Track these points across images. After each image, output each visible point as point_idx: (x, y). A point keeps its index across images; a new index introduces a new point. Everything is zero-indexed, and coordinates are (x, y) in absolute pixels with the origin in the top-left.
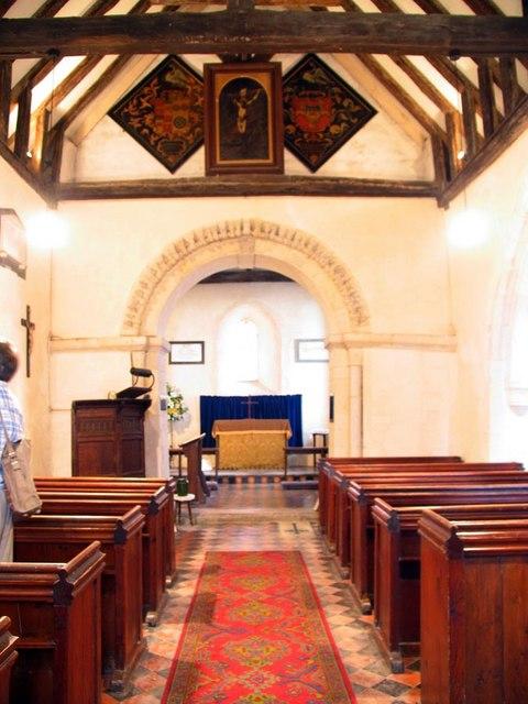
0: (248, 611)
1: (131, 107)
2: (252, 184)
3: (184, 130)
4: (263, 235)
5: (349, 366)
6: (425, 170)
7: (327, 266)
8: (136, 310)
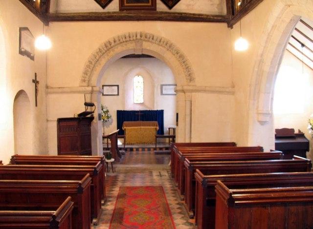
0: (138, 217)
2: (141, 15)
4: (146, 39)
5: (186, 101)
6: (222, 9)
7: (176, 54)
8: (87, 75)
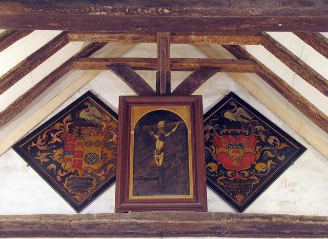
2: (170, 222)
3: (95, 167)
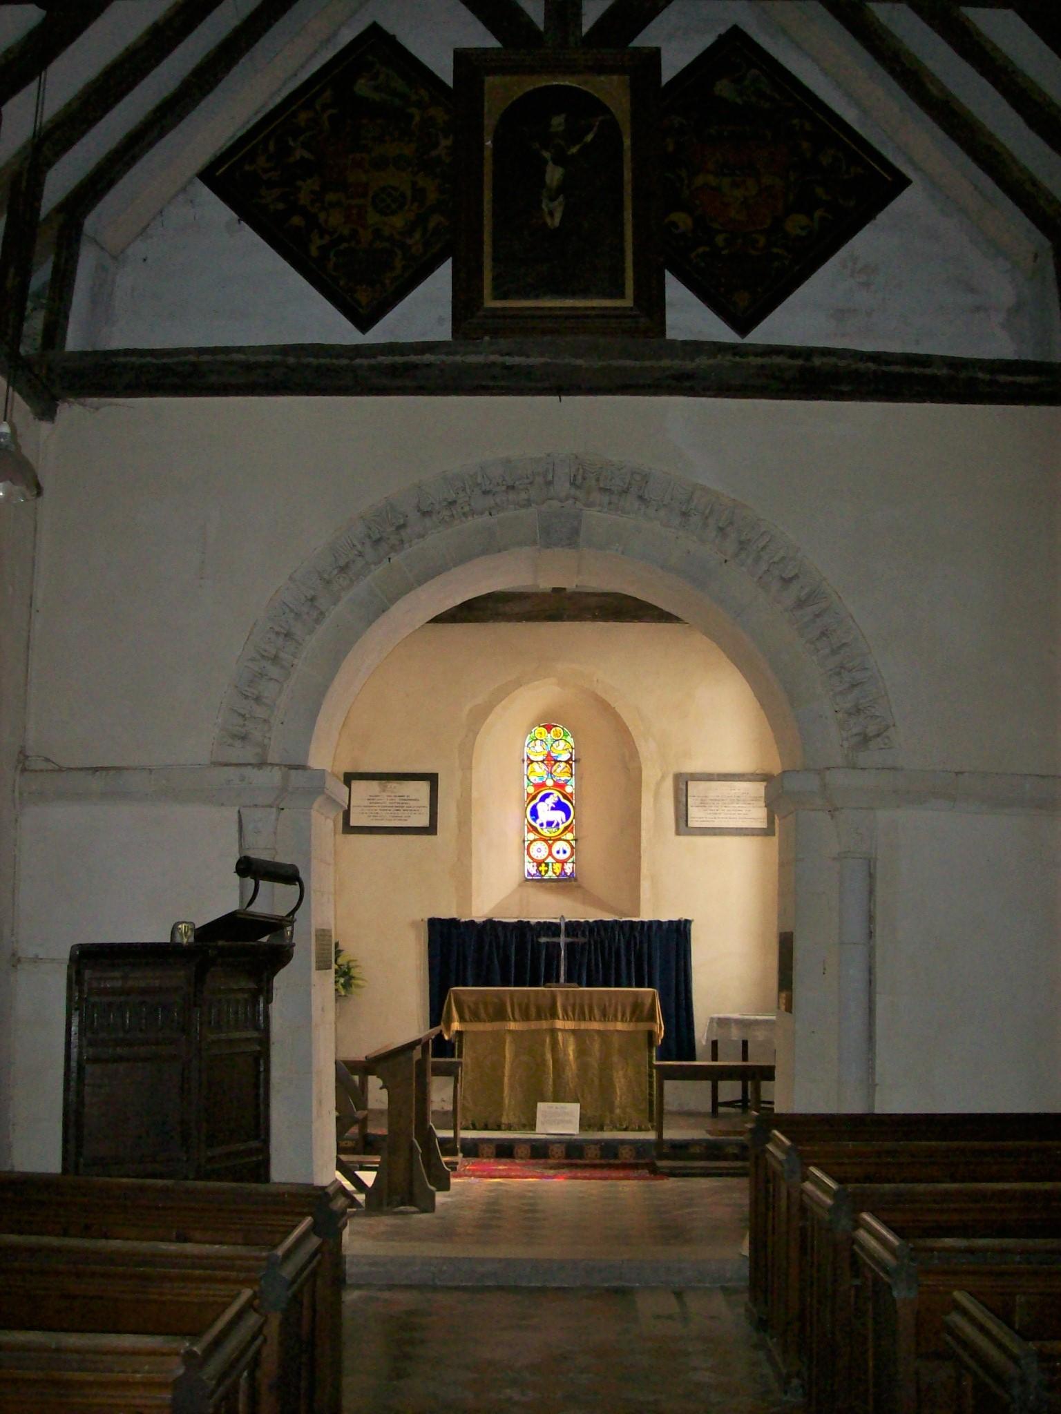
1: (262, 161)
3: (398, 221)
